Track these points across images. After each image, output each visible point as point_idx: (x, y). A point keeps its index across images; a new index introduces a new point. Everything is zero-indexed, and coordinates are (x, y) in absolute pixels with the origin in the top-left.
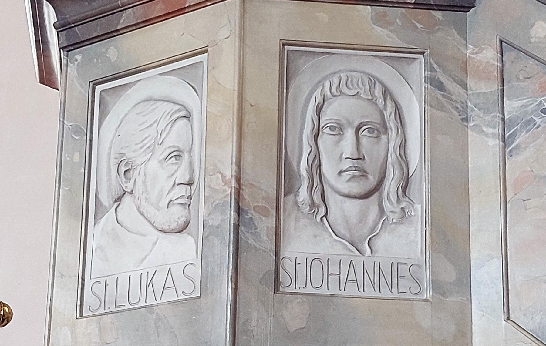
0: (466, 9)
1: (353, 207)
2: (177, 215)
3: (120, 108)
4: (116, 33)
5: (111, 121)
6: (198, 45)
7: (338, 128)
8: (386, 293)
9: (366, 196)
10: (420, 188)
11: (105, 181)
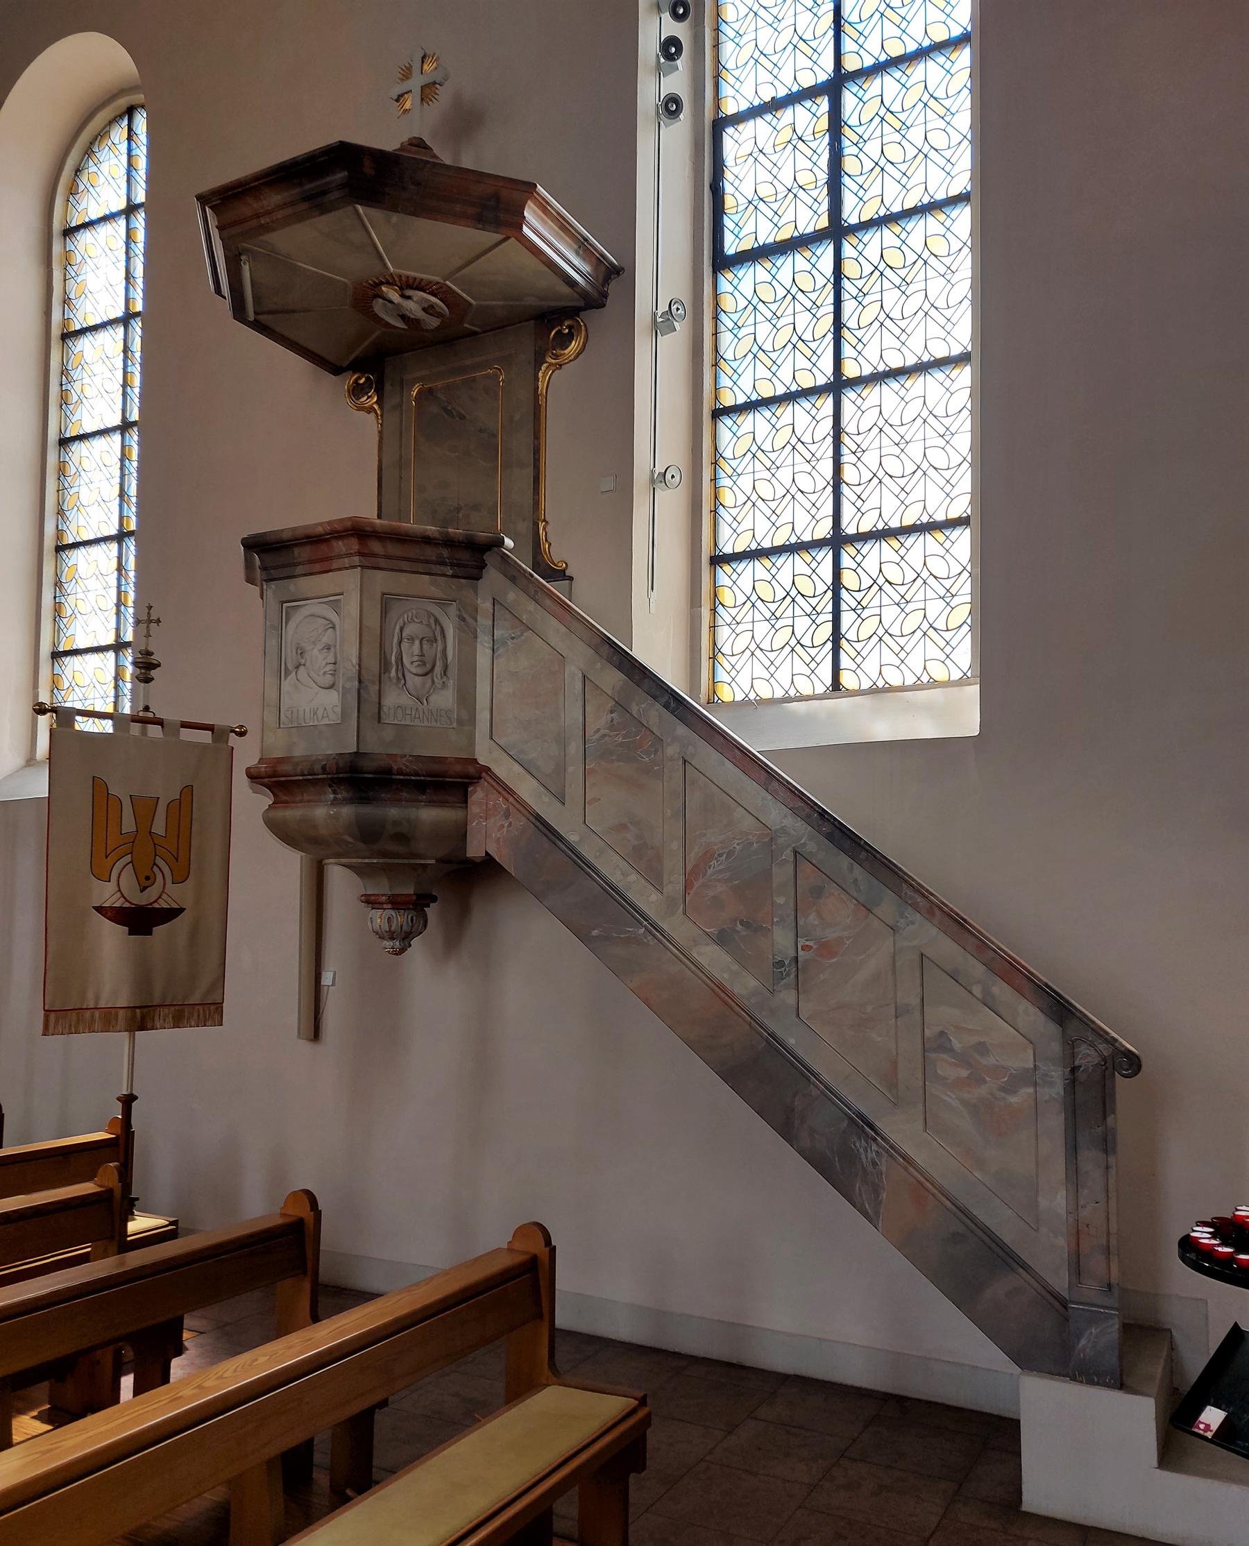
0: (478, 579)
1: (418, 680)
2: (328, 680)
3: (297, 618)
4: (295, 577)
5: (292, 624)
6: (339, 591)
7: (411, 639)
8: (434, 724)
9: (426, 674)
10: (453, 671)
11: (290, 657)
